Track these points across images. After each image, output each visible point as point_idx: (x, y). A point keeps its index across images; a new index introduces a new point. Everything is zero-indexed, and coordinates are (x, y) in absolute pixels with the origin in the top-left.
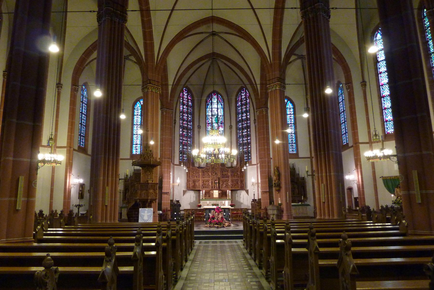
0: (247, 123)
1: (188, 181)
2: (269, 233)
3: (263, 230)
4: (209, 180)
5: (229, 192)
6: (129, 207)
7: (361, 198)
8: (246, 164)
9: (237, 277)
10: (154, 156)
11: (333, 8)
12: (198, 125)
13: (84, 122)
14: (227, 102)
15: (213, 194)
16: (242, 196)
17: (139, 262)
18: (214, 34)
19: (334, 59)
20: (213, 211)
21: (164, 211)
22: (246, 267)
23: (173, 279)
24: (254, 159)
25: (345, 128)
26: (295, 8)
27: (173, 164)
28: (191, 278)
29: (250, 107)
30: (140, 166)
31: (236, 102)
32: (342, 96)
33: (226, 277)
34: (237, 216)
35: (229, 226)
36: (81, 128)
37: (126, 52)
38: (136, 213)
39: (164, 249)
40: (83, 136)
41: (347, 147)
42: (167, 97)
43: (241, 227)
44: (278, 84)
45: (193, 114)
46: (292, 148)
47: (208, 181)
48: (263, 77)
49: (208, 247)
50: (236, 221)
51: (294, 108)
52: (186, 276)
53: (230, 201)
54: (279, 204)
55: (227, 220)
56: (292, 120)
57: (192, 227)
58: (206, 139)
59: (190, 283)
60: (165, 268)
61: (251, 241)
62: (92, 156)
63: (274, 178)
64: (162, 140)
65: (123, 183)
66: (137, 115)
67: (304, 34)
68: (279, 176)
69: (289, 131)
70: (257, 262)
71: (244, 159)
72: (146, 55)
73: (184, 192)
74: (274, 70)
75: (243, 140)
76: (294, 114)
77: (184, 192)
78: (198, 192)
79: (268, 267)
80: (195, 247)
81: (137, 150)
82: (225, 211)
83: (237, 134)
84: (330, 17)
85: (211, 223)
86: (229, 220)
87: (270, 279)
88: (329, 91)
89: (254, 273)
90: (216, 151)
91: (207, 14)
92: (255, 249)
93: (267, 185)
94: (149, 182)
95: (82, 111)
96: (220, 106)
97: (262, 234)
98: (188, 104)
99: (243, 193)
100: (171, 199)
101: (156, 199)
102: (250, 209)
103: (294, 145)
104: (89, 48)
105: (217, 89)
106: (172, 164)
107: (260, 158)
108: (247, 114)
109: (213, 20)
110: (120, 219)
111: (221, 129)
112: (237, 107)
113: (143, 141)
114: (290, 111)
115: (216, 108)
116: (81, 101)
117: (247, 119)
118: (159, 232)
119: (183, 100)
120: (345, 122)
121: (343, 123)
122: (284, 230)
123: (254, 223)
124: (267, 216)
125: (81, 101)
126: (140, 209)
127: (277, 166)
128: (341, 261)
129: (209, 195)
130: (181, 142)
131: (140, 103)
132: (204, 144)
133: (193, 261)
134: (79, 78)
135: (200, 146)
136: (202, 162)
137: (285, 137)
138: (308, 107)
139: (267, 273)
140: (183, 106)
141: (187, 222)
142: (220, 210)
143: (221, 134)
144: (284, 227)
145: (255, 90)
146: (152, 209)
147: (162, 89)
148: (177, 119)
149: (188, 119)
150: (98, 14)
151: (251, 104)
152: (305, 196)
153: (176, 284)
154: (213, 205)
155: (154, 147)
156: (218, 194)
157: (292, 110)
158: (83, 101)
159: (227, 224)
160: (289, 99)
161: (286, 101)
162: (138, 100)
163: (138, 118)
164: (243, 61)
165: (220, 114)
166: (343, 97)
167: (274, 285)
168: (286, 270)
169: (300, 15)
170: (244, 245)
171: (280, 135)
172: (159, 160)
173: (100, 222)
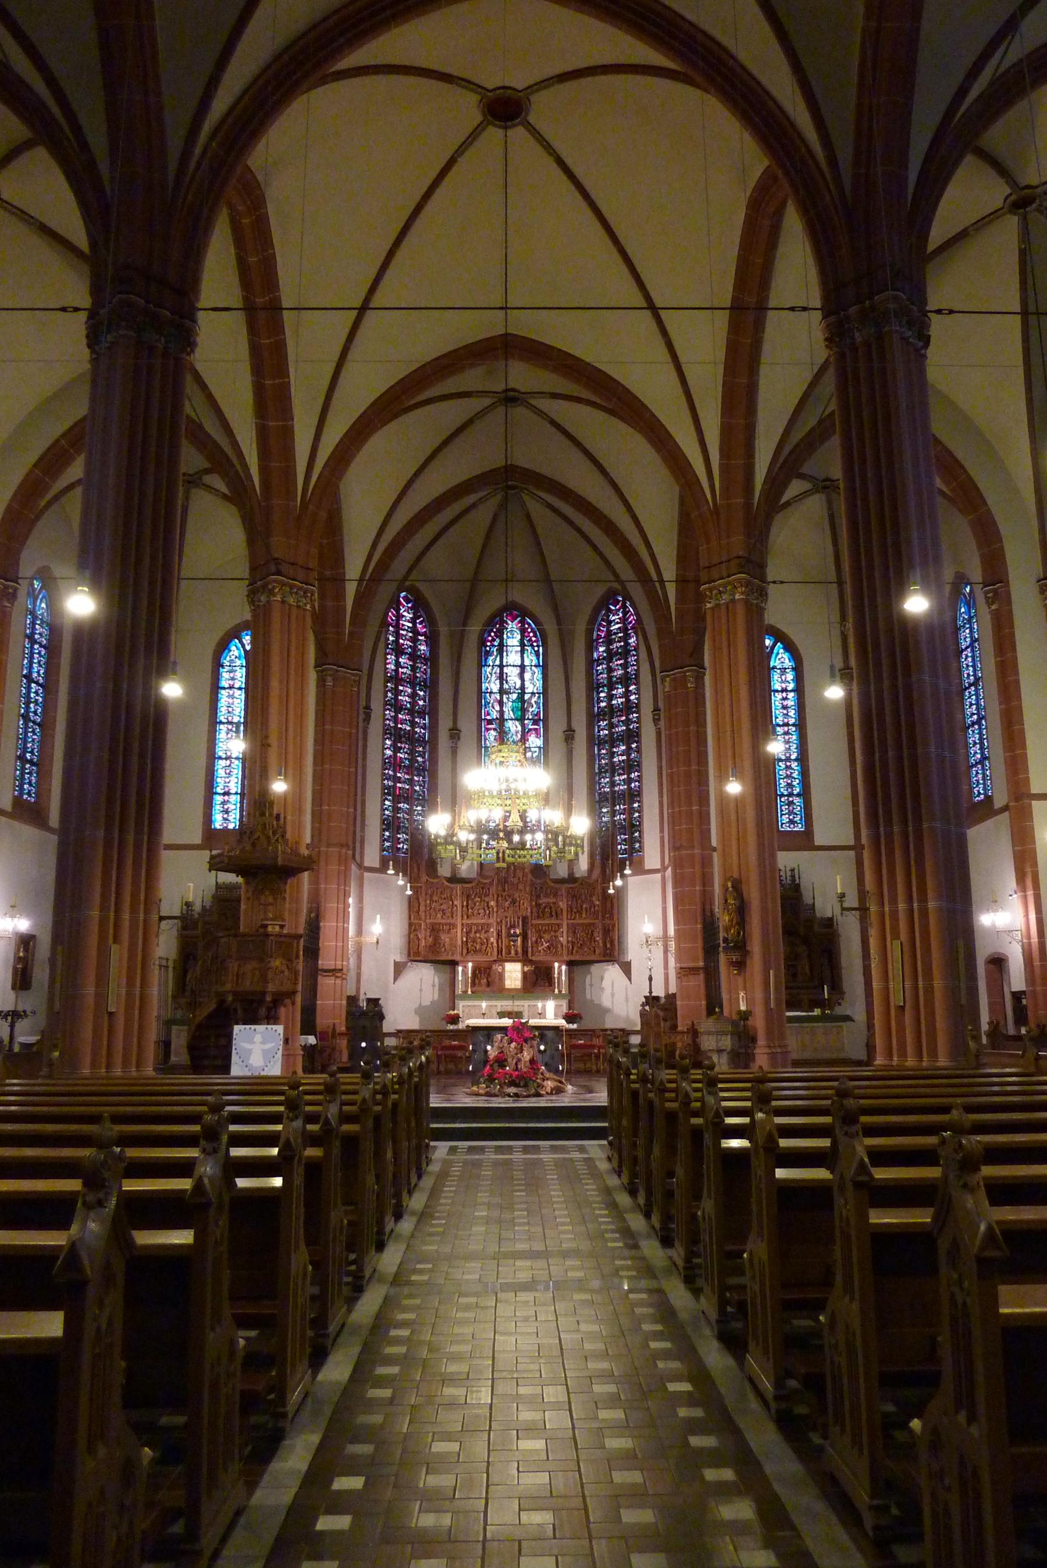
0: (628, 722)
1: (412, 928)
2: (696, 1114)
3: (675, 1105)
4: (489, 925)
5: (560, 970)
6: (198, 1019)
7: (1034, 992)
8: (622, 868)
9: (580, 1274)
10: (288, 836)
11: (939, 312)
12: (450, 725)
13: (35, 713)
14: (557, 647)
15: (501, 976)
16: (606, 983)
17: (212, 1211)
18: (510, 398)
19: (941, 492)
20: (499, 1036)
21: (322, 1037)
22: (614, 1240)
23: (349, 1279)
24: (652, 853)
25: (982, 744)
26: (804, 309)
27: (360, 866)
28: (413, 1278)
29: (639, 663)
30: (238, 872)
31: (591, 646)
32: (971, 629)
33: (542, 1275)
34: (590, 1055)
35: (558, 1091)
36: (26, 733)
37: (191, 459)
38: (223, 1041)
39: (313, 1169)
40: (31, 762)
41: (986, 809)
42: (339, 624)
43: (600, 1097)
44: (739, 580)
45: (432, 686)
46: (790, 813)
47: (485, 928)
48: (685, 556)
49: (478, 1164)
50: (587, 1072)
51: (798, 670)
52: (394, 1269)
53: (564, 1004)
54: (740, 1012)
55: (549, 1071)
56: (792, 713)
57: (420, 1093)
58: (476, 778)
59: (411, 1296)
60: (315, 1235)
61: (635, 1145)
62: (63, 832)
63: (724, 919)
64: (318, 778)
65: (175, 933)
66: (231, 687)
67: (833, 406)
68: (741, 911)
69: (775, 747)
70: (655, 1220)
71: (615, 849)
72: (263, 469)
73: (399, 969)
74: (730, 532)
75: (613, 784)
76: (799, 690)
77: (399, 969)
78: (447, 968)
79: (693, 1239)
80: (434, 1168)
81: (227, 815)
82: (542, 1038)
83: (591, 758)
84: (927, 341)
85: (491, 1079)
86: (556, 1071)
87: (700, 1282)
88: (916, 604)
89: (643, 1259)
90: (515, 820)
91: (489, 326)
92: (649, 1175)
93: (700, 944)
94: (270, 929)
95: (30, 672)
96: (530, 659)
97: (671, 1117)
98: (415, 648)
99: (612, 973)
100: (351, 992)
101: (294, 993)
102: (636, 1033)
103: (797, 801)
104: (57, 441)
105: (519, 595)
106: (354, 867)
107: (675, 848)
108: (627, 687)
109: (507, 347)
110: (164, 1064)
111: (535, 742)
112: (591, 663)
113: (252, 778)
114: (782, 680)
115: (515, 665)
116: (27, 636)
117: (628, 707)
118: (293, 1105)
119: (398, 636)
120: (980, 719)
121: (973, 724)
122: (748, 1104)
123: (644, 1079)
124: (697, 1058)
125: (27, 636)
126: (237, 1028)
127: (736, 875)
128: (945, 1211)
129: (486, 980)
130: (389, 788)
131: (243, 646)
132: (469, 792)
133: (424, 1216)
134: (19, 552)
135: (455, 800)
136: (463, 858)
137: (763, 772)
138: (847, 667)
139: (688, 1260)
140: (397, 657)
141: (400, 1076)
142: (527, 1034)
143: (534, 761)
144: (748, 1094)
145: (658, 603)
146: (280, 1029)
147: (322, 597)
148: (376, 705)
149: (414, 703)
150: (90, 317)
151: (643, 649)
152: (836, 987)
153: (357, 1299)
154: (501, 1015)
155: (289, 800)
156: (519, 975)
157: (790, 676)
158: (33, 633)
159: (549, 1084)
160: (780, 637)
161: (768, 642)
162: (235, 634)
163: (232, 697)
164: (622, 509)
165: (530, 688)
166: (973, 631)
167: (715, 1300)
168: (757, 1249)
169: (819, 335)
170: (609, 1159)
171: (747, 764)
172: (306, 852)
173: (86, 1071)
